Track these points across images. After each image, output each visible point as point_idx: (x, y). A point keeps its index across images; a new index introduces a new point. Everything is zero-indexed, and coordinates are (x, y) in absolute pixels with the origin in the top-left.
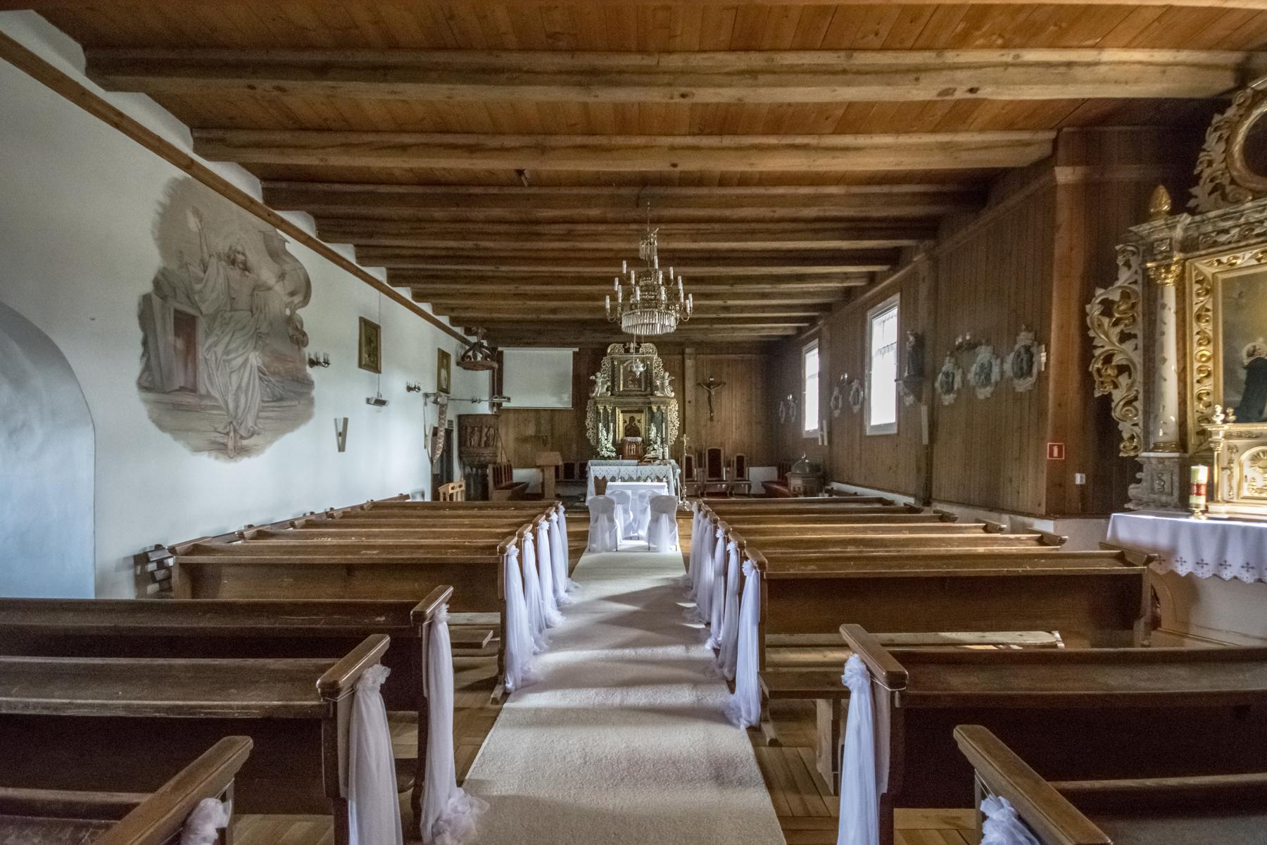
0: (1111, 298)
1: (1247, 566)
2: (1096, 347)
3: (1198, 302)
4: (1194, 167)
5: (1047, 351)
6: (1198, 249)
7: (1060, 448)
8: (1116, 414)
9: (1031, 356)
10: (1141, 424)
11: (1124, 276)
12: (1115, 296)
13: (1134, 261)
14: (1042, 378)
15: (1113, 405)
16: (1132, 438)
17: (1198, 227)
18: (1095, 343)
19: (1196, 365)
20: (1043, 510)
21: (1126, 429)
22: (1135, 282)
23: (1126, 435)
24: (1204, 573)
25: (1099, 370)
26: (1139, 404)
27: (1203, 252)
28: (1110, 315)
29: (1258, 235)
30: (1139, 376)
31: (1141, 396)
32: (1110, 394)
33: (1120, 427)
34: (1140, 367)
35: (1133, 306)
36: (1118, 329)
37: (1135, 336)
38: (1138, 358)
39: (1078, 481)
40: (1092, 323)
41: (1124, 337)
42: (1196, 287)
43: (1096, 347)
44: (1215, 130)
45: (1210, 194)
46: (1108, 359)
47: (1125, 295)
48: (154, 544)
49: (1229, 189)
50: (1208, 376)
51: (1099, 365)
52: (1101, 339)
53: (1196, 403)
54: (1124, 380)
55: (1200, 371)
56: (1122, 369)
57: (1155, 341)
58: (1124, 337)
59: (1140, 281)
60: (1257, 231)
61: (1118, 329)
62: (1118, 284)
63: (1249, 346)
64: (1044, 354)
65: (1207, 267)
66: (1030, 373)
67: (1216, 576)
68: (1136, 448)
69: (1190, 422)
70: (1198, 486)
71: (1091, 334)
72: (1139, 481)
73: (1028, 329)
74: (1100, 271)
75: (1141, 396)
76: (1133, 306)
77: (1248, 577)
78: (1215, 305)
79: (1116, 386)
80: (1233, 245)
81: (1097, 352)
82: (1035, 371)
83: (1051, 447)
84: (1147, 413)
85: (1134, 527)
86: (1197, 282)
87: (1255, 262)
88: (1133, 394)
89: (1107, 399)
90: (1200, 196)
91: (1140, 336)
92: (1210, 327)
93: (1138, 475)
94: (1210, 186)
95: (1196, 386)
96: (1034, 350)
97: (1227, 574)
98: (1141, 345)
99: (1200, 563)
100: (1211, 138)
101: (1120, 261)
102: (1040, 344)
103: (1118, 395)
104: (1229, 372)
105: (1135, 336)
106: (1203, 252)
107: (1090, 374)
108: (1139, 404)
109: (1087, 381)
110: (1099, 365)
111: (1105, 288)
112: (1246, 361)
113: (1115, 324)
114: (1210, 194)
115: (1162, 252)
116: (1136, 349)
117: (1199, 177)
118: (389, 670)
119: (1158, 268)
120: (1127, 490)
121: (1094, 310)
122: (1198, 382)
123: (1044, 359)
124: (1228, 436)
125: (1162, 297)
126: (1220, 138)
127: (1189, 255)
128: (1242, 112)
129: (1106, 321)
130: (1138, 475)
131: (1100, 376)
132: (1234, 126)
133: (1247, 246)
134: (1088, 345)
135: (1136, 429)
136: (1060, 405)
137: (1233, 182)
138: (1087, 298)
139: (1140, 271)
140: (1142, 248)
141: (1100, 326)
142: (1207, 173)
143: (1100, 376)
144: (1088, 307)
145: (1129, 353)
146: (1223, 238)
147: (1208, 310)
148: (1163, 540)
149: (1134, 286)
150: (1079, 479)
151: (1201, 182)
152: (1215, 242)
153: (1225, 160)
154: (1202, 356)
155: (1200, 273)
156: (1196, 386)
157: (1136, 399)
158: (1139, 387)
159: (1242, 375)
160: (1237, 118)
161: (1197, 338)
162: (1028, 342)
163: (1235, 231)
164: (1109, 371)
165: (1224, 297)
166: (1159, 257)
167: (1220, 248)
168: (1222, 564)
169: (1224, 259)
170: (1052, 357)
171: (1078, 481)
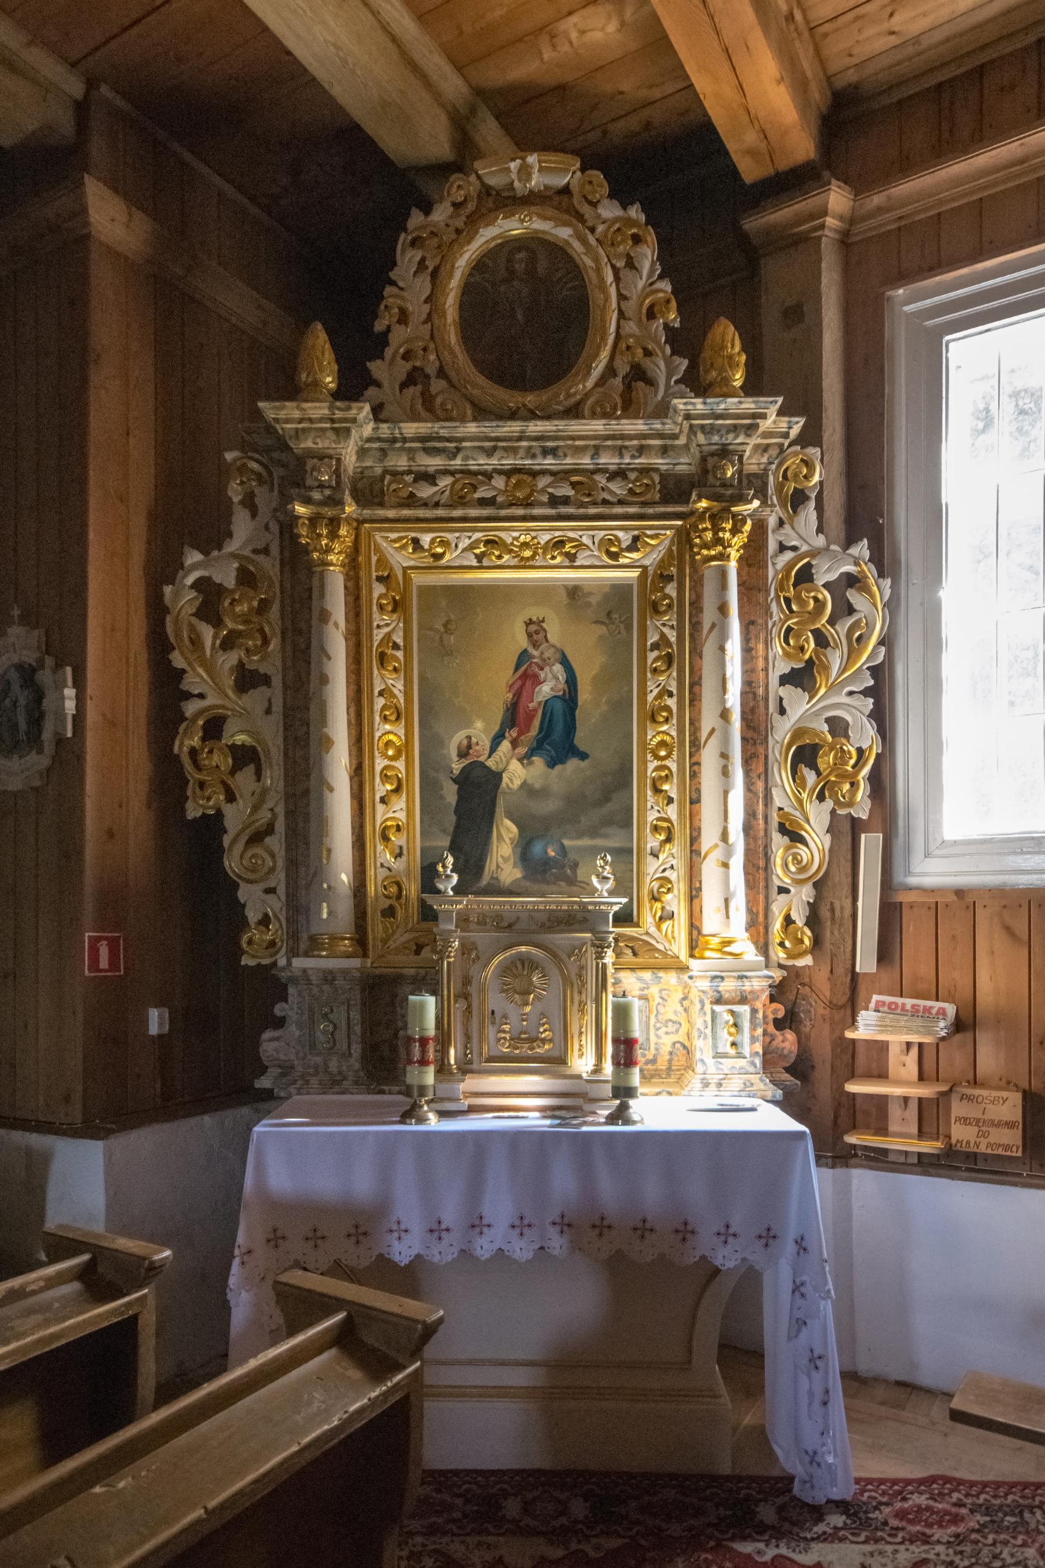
0: (217, 579)
1: (521, 1225)
2: (188, 696)
3: (384, 626)
4: (375, 316)
5: (79, 683)
6: (381, 505)
7: (113, 944)
8: (232, 864)
9: (39, 696)
10: (281, 890)
11: (243, 530)
12: (226, 576)
13: (264, 498)
14: (69, 754)
15: (226, 841)
16: (265, 921)
17: (383, 452)
18: (184, 686)
19: (380, 763)
20: (76, 1113)
21: (253, 900)
22: (266, 551)
23: (252, 916)
24: (442, 1253)
25: (193, 752)
26: (276, 842)
27: (391, 514)
28: (217, 622)
29: (483, 502)
30: (273, 777)
31: (280, 825)
32: (219, 814)
33: (242, 895)
34: (276, 754)
35: (264, 606)
36: (232, 658)
37: (266, 680)
38: (271, 736)
39: (154, 1029)
40: (178, 635)
41: (247, 680)
42: (379, 589)
43: (188, 696)
44: (414, 243)
45: (404, 386)
46: (214, 728)
47: (247, 578)
48: (720, 720)
49: (437, 385)
50: (397, 790)
51: (195, 741)
52: (196, 680)
53: (380, 847)
54: (244, 781)
55: (385, 778)
56: (246, 757)
57: (307, 699)
58: (247, 680)
59: (275, 550)
60: (482, 493)
61: (232, 658)
62: (232, 546)
63: (458, 738)
64: (70, 692)
65: (394, 549)
66: (35, 741)
67: (465, 1254)
68: (272, 944)
69: (371, 889)
70: (424, 1041)
71: (178, 660)
72: (280, 1023)
73: (28, 620)
74: (186, 517)
75: (280, 825)
76: (264, 606)
77: (522, 1250)
78: (407, 637)
79: (231, 798)
80: (440, 512)
81: (191, 708)
82: (47, 735)
83: (94, 942)
84: (293, 864)
85: (299, 1152)
86: (379, 579)
87: (474, 563)
88: (264, 816)
89: (214, 823)
90: (386, 384)
91: (277, 681)
92: (400, 685)
93: (279, 1010)
94: (403, 368)
95: (380, 808)
96: (45, 676)
97: (484, 1247)
98: (278, 707)
99: (437, 1230)
100: (407, 259)
101: (235, 491)
102: (59, 666)
103: (234, 817)
104: (429, 785)
105: (266, 680)
106: (391, 514)
107: (177, 758)
108: (276, 842)
109: (169, 780)
110: (195, 741)
111: (206, 553)
112: (457, 767)
113: (227, 644)
114: (404, 386)
115: (321, 486)
116: (268, 712)
117: (383, 339)
118: (170, 657)
119: (314, 521)
120: (256, 1044)
121: (183, 599)
122: (383, 800)
123: (70, 706)
124: (463, 921)
125: (322, 596)
126: (422, 264)
127: (367, 513)
128: (459, 223)
129: (207, 633)
130: (279, 1010)
131: (198, 768)
132: (447, 251)
133: (464, 519)
134: (167, 689)
135: (271, 898)
136: (111, 834)
137: (442, 373)
138: (162, 570)
139: (274, 527)
140: (277, 472)
141: (196, 642)
142: (399, 336)
143: (198, 768)
144: (168, 590)
145: (251, 722)
146: (425, 492)
147: (396, 647)
148: (362, 1185)
149: (261, 558)
150: (156, 1021)
151: (388, 352)
152: (412, 495)
153: (429, 318)
154: (389, 744)
155: (382, 562)
156: (380, 808)
157: (269, 830)
158: (276, 805)
159: (450, 793)
160: (449, 236)
161: (380, 702)
162: (30, 657)
163: (445, 482)
164: (216, 759)
165: (421, 627)
166: (317, 495)
167: (421, 513)
168: (477, 1225)
169: (426, 539)
170: (90, 706)
171: (154, 1029)
